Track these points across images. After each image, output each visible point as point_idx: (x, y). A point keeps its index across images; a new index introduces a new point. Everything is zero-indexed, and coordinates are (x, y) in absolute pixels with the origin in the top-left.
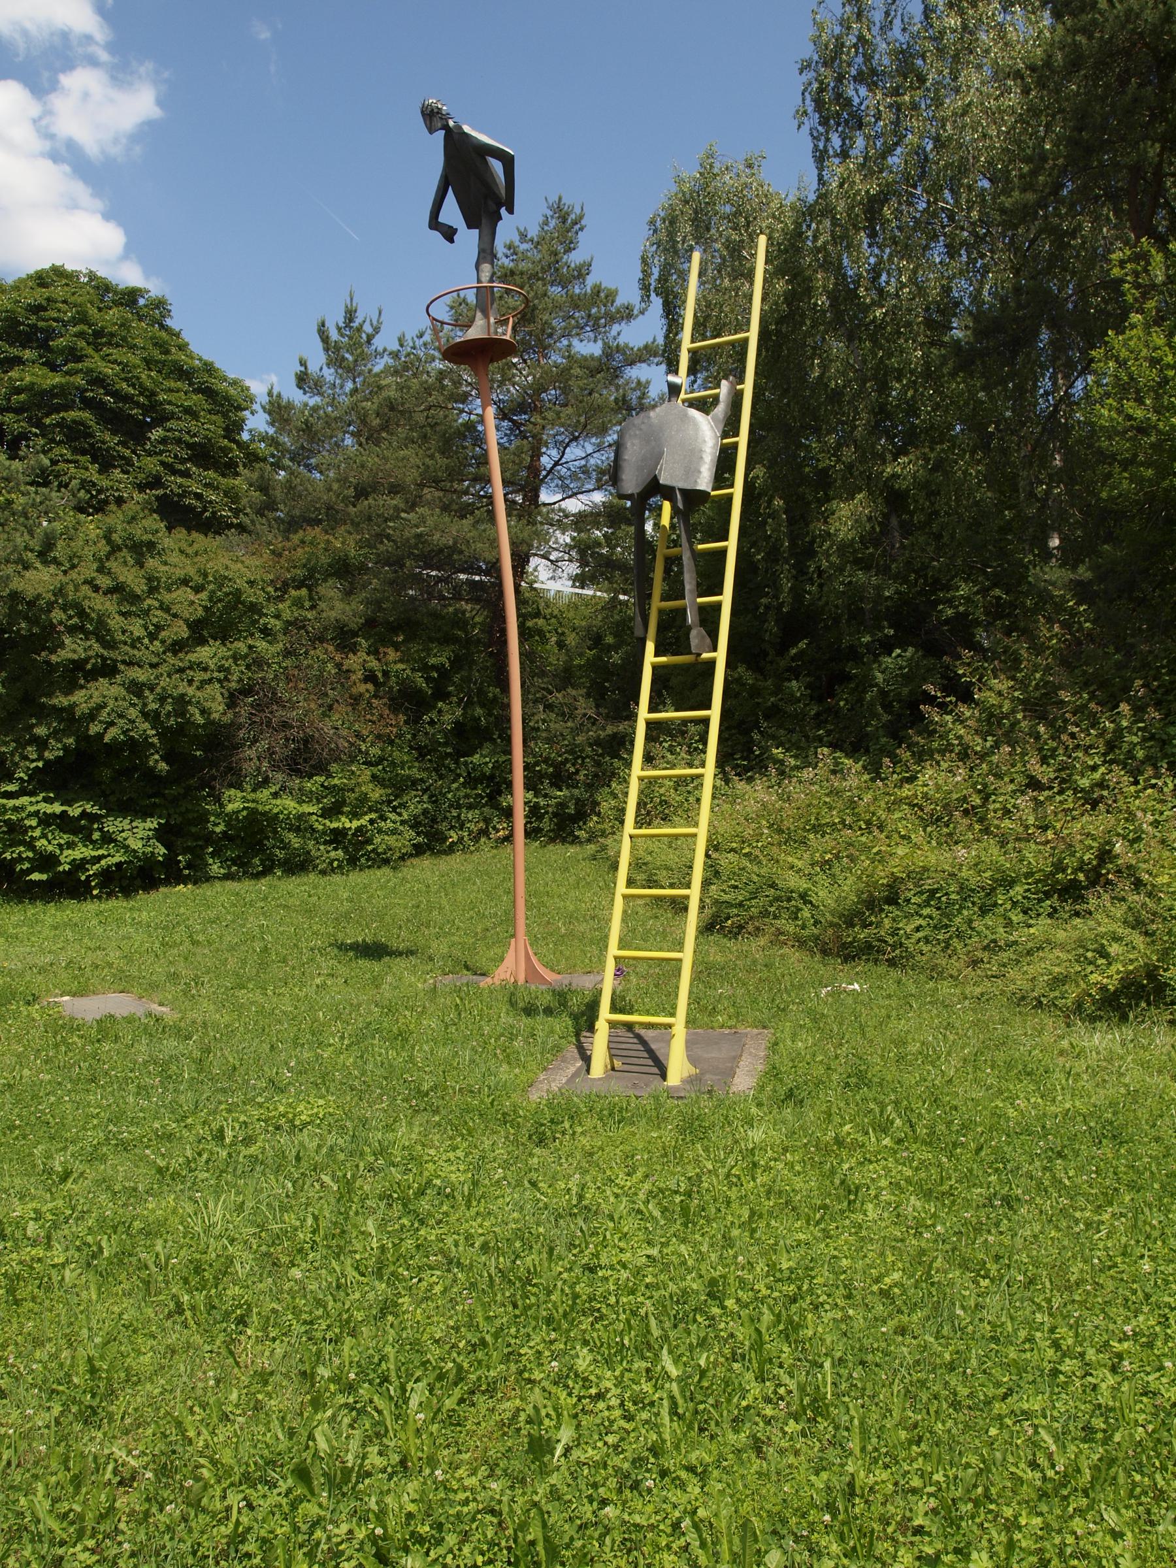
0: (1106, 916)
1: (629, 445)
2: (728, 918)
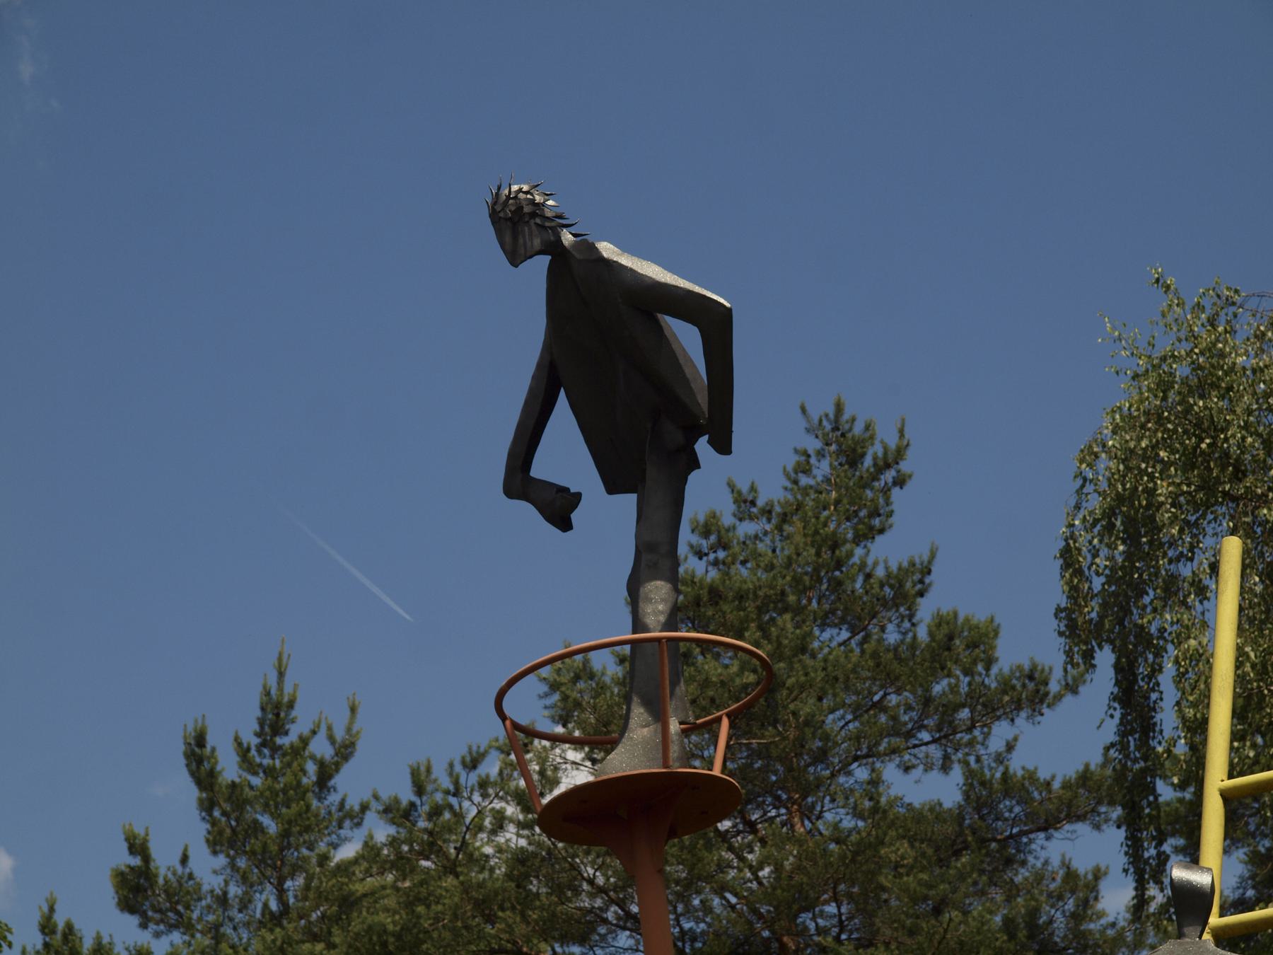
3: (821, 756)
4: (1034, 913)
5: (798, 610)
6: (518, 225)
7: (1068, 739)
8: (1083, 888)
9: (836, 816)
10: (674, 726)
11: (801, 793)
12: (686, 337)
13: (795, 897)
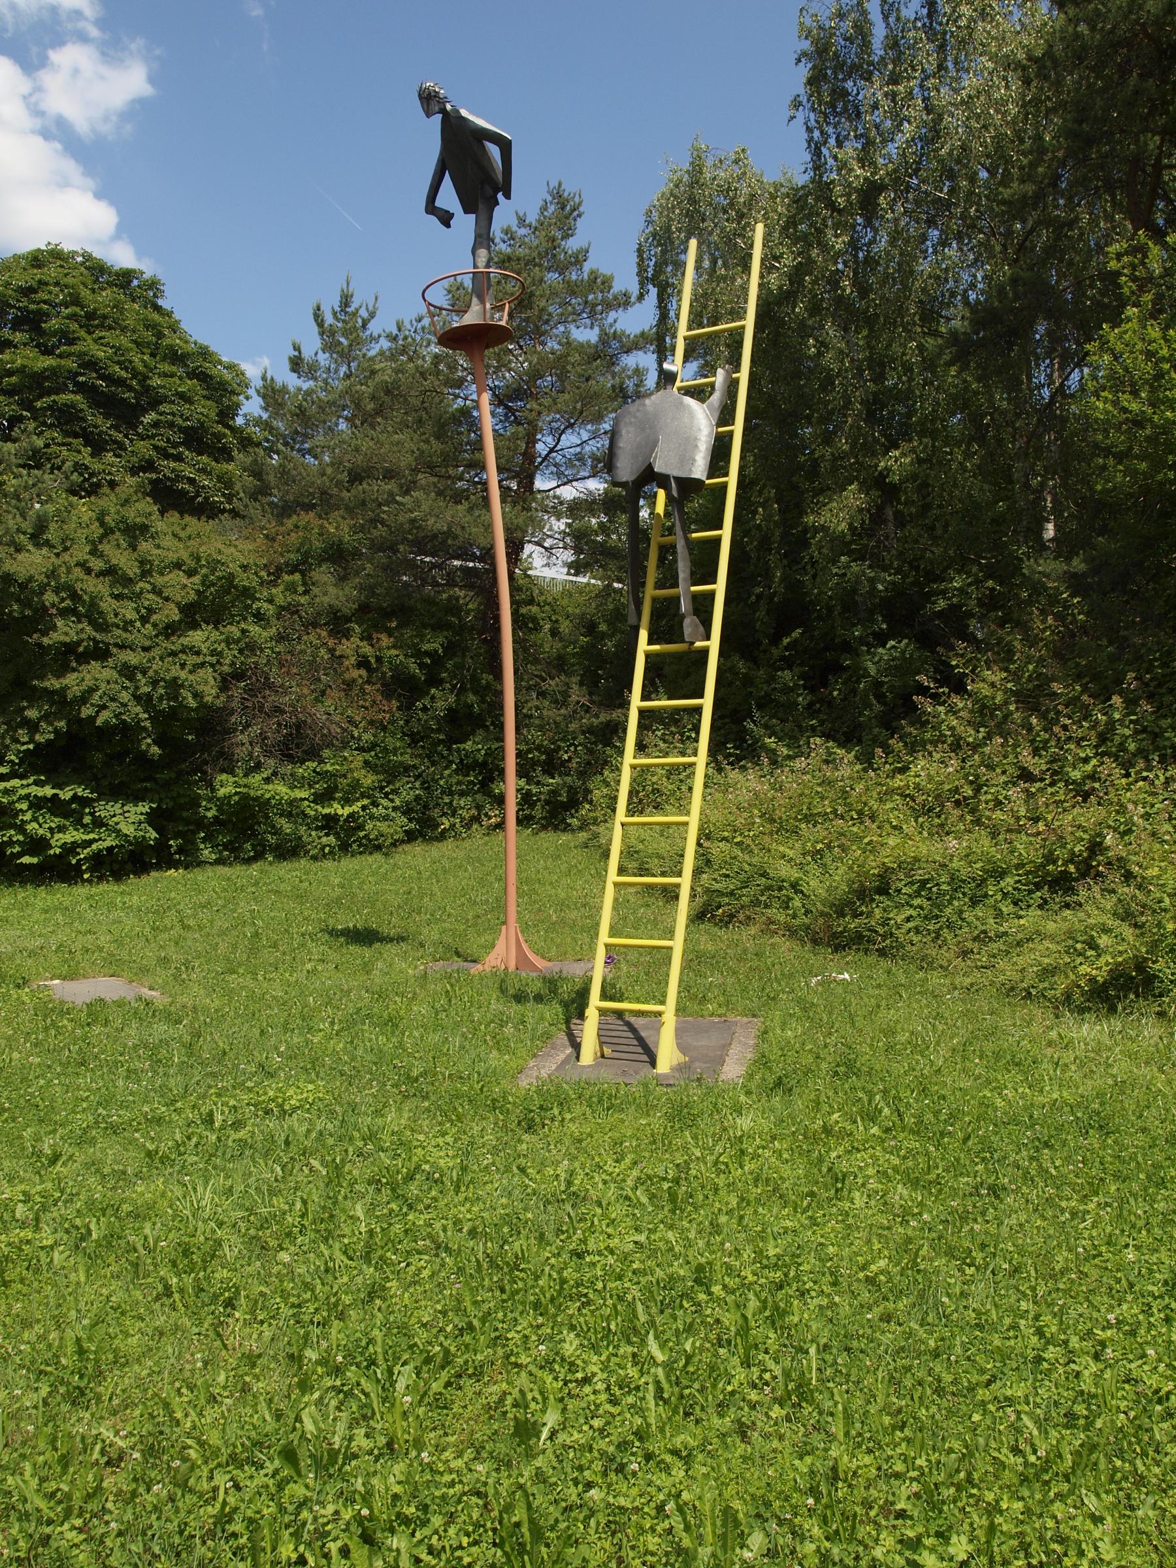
0: (1096, 908)
1: (624, 432)
2: (719, 907)
3: (547, 322)
4: (622, 383)
5: (540, 265)
6: (429, 100)
7: (638, 319)
8: (639, 372)
9: (552, 345)
10: (488, 306)
11: (539, 334)
12: (494, 151)
13: (535, 374)
